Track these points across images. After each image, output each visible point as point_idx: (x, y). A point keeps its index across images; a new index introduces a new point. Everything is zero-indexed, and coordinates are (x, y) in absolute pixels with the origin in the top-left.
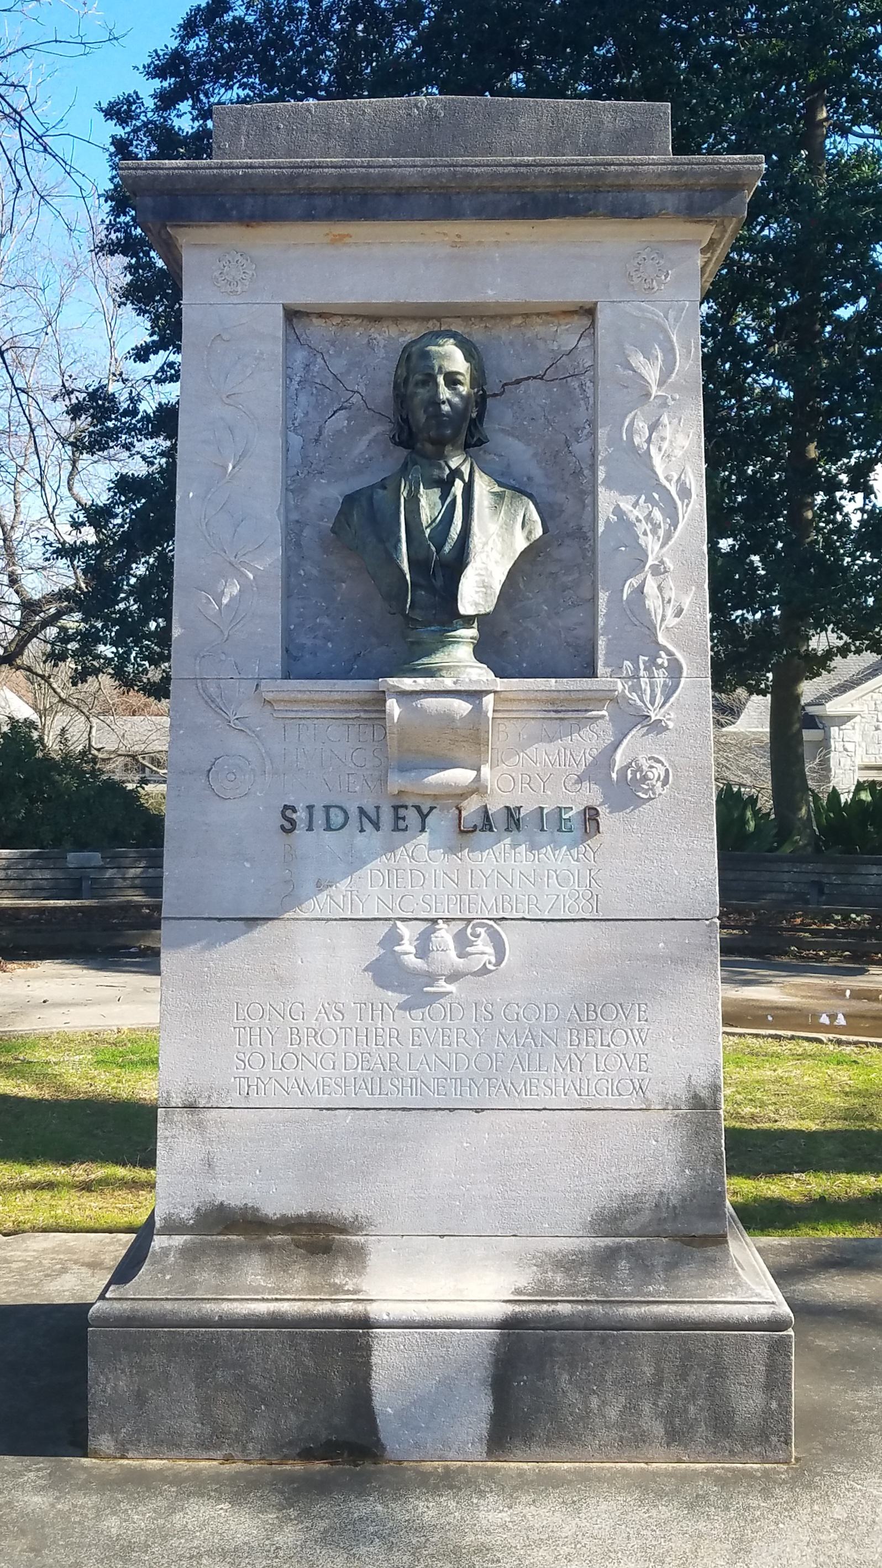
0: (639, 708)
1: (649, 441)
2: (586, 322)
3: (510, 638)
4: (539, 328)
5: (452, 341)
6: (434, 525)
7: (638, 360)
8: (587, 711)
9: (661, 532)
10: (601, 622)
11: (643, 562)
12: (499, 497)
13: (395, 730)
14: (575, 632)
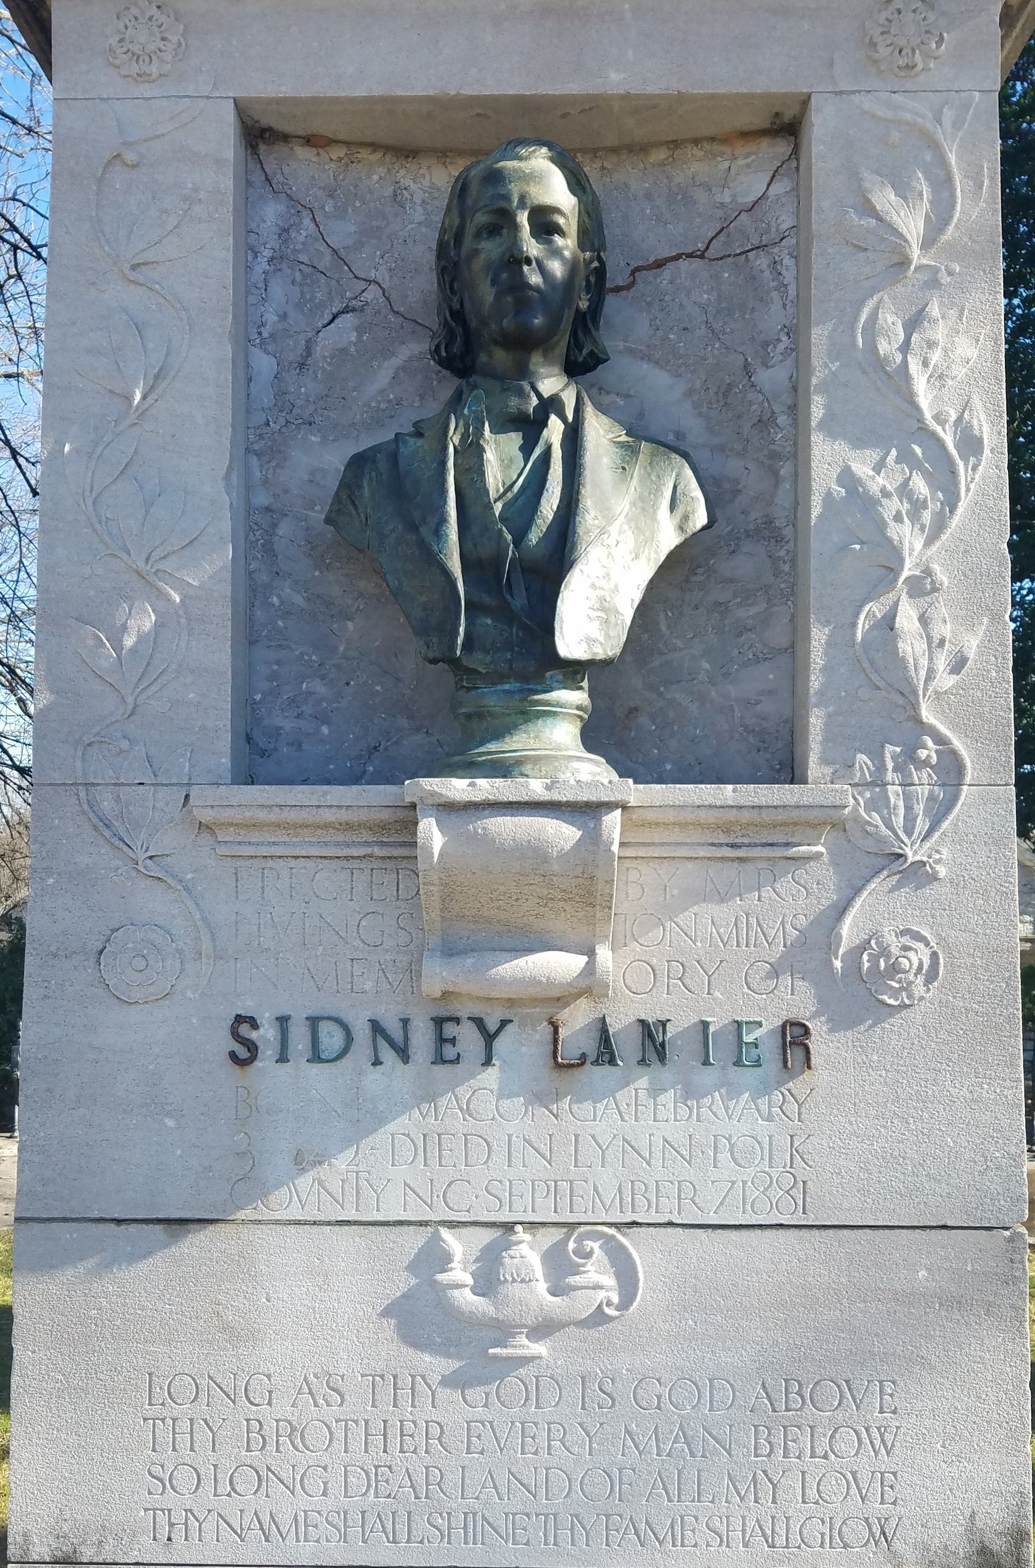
0: (881, 840)
1: (905, 348)
2: (782, 148)
3: (643, 720)
4: (696, 166)
5: (544, 150)
6: (510, 495)
7: (885, 199)
8: (787, 845)
9: (927, 516)
10: (815, 682)
11: (892, 571)
12: (630, 451)
13: (435, 879)
14: (759, 708)
